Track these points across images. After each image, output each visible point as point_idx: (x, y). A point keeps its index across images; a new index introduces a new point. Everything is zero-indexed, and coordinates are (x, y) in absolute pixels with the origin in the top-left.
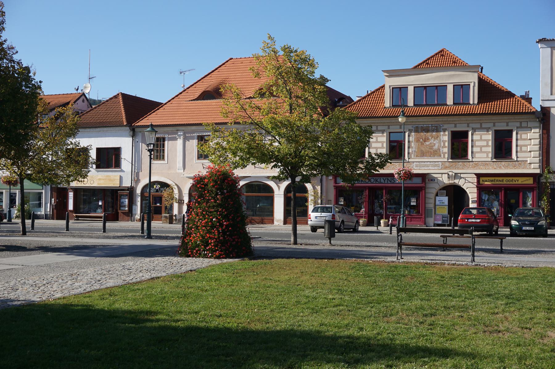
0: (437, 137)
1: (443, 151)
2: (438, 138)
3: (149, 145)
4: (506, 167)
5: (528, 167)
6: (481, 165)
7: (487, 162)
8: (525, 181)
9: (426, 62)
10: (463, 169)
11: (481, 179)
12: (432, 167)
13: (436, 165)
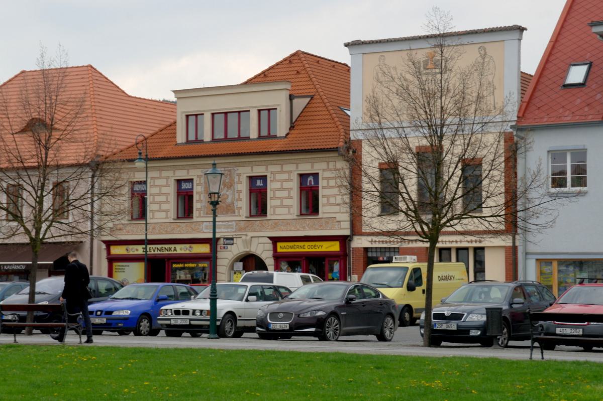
0: (231, 186)
1: (237, 205)
2: (232, 188)
3: (213, 195)
4: (312, 228)
5: (336, 226)
6: (281, 225)
7: (289, 221)
8: (330, 246)
9: (264, 74)
10: (260, 231)
11: (279, 245)
12: (224, 228)
13: (229, 225)
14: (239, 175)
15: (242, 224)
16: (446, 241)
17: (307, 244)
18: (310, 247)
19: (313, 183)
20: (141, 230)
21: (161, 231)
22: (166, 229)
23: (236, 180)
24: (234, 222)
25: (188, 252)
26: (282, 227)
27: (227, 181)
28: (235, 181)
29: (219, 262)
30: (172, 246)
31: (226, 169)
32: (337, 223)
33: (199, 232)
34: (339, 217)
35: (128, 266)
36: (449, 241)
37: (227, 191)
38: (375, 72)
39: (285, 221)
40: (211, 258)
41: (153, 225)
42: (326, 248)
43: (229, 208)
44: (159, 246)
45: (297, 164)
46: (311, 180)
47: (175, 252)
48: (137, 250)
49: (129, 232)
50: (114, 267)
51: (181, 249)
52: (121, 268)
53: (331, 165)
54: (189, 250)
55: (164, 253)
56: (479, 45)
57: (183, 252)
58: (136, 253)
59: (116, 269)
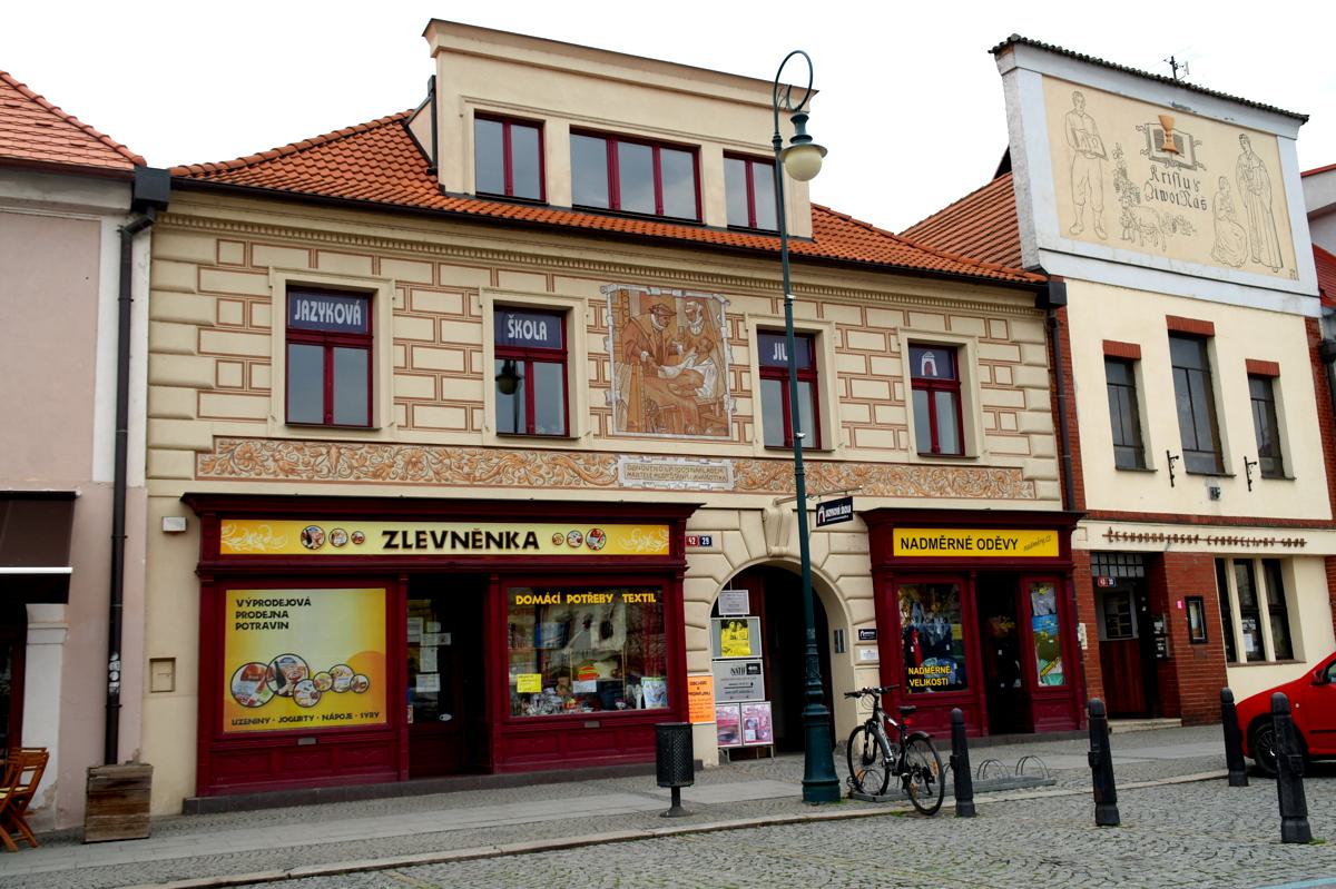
2: (714, 354)
4: (962, 491)
6: (879, 480)
7: (898, 469)
8: (1036, 544)
14: (737, 319)
15: (757, 470)
16: (1248, 541)
17: (976, 535)
18: (986, 544)
19: (935, 373)
20: (351, 467)
21: (447, 474)
22: (466, 469)
23: (726, 332)
24: (727, 461)
25: (583, 550)
26: (881, 485)
27: (695, 330)
28: (724, 335)
29: (691, 588)
30: (522, 530)
31: (689, 294)
32: (1026, 484)
33: (603, 486)
34: (1033, 467)
35: (308, 603)
36: (1254, 541)
37: (697, 363)
38: (1069, 127)
39: (887, 468)
40: (665, 576)
41: (408, 450)
42: (1026, 548)
43: (708, 415)
44: (462, 529)
45: (864, 310)
46: (928, 364)
47: (531, 551)
48: (358, 540)
49: (293, 471)
50: (231, 609)
51: (552, 541)
52: (269, 609)
53: (998, 330)
54: (589, 545)
55: (484, 551)
56: (1243, 132)
57: (564, 550)
58: (351, 549)
59: (238, 615)
